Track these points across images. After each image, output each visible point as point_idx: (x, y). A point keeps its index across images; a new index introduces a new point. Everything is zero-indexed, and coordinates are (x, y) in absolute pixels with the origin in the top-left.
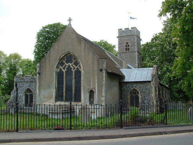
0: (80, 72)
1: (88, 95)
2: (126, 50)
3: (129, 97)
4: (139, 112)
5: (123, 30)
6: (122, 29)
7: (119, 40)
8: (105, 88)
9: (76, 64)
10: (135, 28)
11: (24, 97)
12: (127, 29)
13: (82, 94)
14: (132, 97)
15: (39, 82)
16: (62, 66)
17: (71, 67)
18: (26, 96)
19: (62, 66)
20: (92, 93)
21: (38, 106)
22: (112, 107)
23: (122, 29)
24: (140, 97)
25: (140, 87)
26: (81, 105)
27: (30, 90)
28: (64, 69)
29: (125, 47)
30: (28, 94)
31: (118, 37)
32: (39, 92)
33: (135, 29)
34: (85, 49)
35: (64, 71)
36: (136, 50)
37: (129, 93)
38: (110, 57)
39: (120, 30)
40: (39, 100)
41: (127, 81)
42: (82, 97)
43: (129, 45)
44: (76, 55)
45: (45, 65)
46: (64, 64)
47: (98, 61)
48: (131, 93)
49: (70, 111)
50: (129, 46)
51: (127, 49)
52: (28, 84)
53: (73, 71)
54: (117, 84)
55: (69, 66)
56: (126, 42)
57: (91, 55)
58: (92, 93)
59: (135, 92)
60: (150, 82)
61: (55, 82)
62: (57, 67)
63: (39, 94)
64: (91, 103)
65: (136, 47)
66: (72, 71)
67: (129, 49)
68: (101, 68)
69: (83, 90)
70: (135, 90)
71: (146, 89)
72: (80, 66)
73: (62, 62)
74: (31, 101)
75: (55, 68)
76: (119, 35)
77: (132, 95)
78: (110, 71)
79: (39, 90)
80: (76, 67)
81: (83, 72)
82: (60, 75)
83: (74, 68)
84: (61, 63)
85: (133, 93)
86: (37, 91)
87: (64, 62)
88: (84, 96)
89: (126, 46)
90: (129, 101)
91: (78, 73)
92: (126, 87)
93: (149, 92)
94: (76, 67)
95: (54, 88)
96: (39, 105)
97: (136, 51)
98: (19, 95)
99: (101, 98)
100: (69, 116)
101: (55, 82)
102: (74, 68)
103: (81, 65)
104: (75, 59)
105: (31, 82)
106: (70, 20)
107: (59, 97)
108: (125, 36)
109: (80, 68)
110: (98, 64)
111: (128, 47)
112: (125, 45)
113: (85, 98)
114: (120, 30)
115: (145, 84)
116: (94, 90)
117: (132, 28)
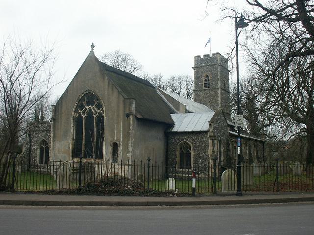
0: (103, 117)
1: (110, 149)
2: (205, 87)
3: (178, 153)
4: (303, 174)
5: (202, 57)
6: (200, 56)
7: (195, 71)
8: (132, 139)
9: (99, 106)
10: (218, 53)
11: (38, 151)
12: (207, 56)
13: (104, 148)
14: (182, 154)
15: (54, 131)
16: (82, 110)
17: (92, 110)
18: (41, 150)
19: (82, 110)
20: (115, 147)
21: (52, 162)
22: (151, 165)
23: (200, 56)
24: (193, 153)
25: (193, 140)
26: (61, 161)
27: (45, 141)
28: (84, 113)
29: (204, 82)
30: (43, 146)
31: (194, 68)
32: (54, 145)
33: (218, 55)
34: (109, 86)
35: (84, 117)
36: (219, 86)
37: (178, 148)
38: (163, 96)
39: (197, 58)
40: (53, 154)
41: (179, 130)
42: (104, 152)
43: (210, 78)
44: (99, 94)
45: (61, 107)
46: (84, 107)
47: (124, 104)
48: (181, 149)
49: (79, 171)
50: (209, 80)
51: (207, 85)
52: (43, 134)
53: (95, 116)
54: (161, 134)
55: (90, 109)
56: (205, 74)
57: (116, 93)
58: (115, 147)
59: (186, 147)
60: (206, 132)
61: (72, 131)
62: (76, 111)
63: (54, 148)
64: (115, 159)
65: (219, 82)
66: (93, 116)
67: (209, 84)
68: (127, 112)
69: (105, 143)
70: (187, 143)
71: (200, 143)
72: (102, 110)
73: (82, 104)
74: (47, 157)
75: (73, 112)
76: (195, 64)
77: (182, 151)
78: (139, 116)
79: (54, 141)
80: (98, 111)
81: (105, 118)
82: (78, 121)
83: (96, 112)
84: (80, 106)
85: (184, 148)
86: (52, 143)
87: (85, 103)
88: (106, 151)
89: (205, 80)
90: (178, 159)
91: (100, 118)
92: (175, 139)
93: (205, 148)
94: (98, 111)
95: (71, 138)
96: (54, 161)
97: (218, 88)
98: (33, 148)
99: (127, 154)
100: (78, 177)
101: (72, 131)
102: (96, 112)
103: (104, 109)
104: (97, 100)
105: (46, 131)
106: (93, 46)
107: (76, 153)
108: (204, 66)
109: (103, 113)
110: (124, 107)
111: (208, 82)
112: (204, 80)
113: (107, 154)
114: (197, 58)
115: (200, 135)
116: (118, 143)
117: (214, 54)
